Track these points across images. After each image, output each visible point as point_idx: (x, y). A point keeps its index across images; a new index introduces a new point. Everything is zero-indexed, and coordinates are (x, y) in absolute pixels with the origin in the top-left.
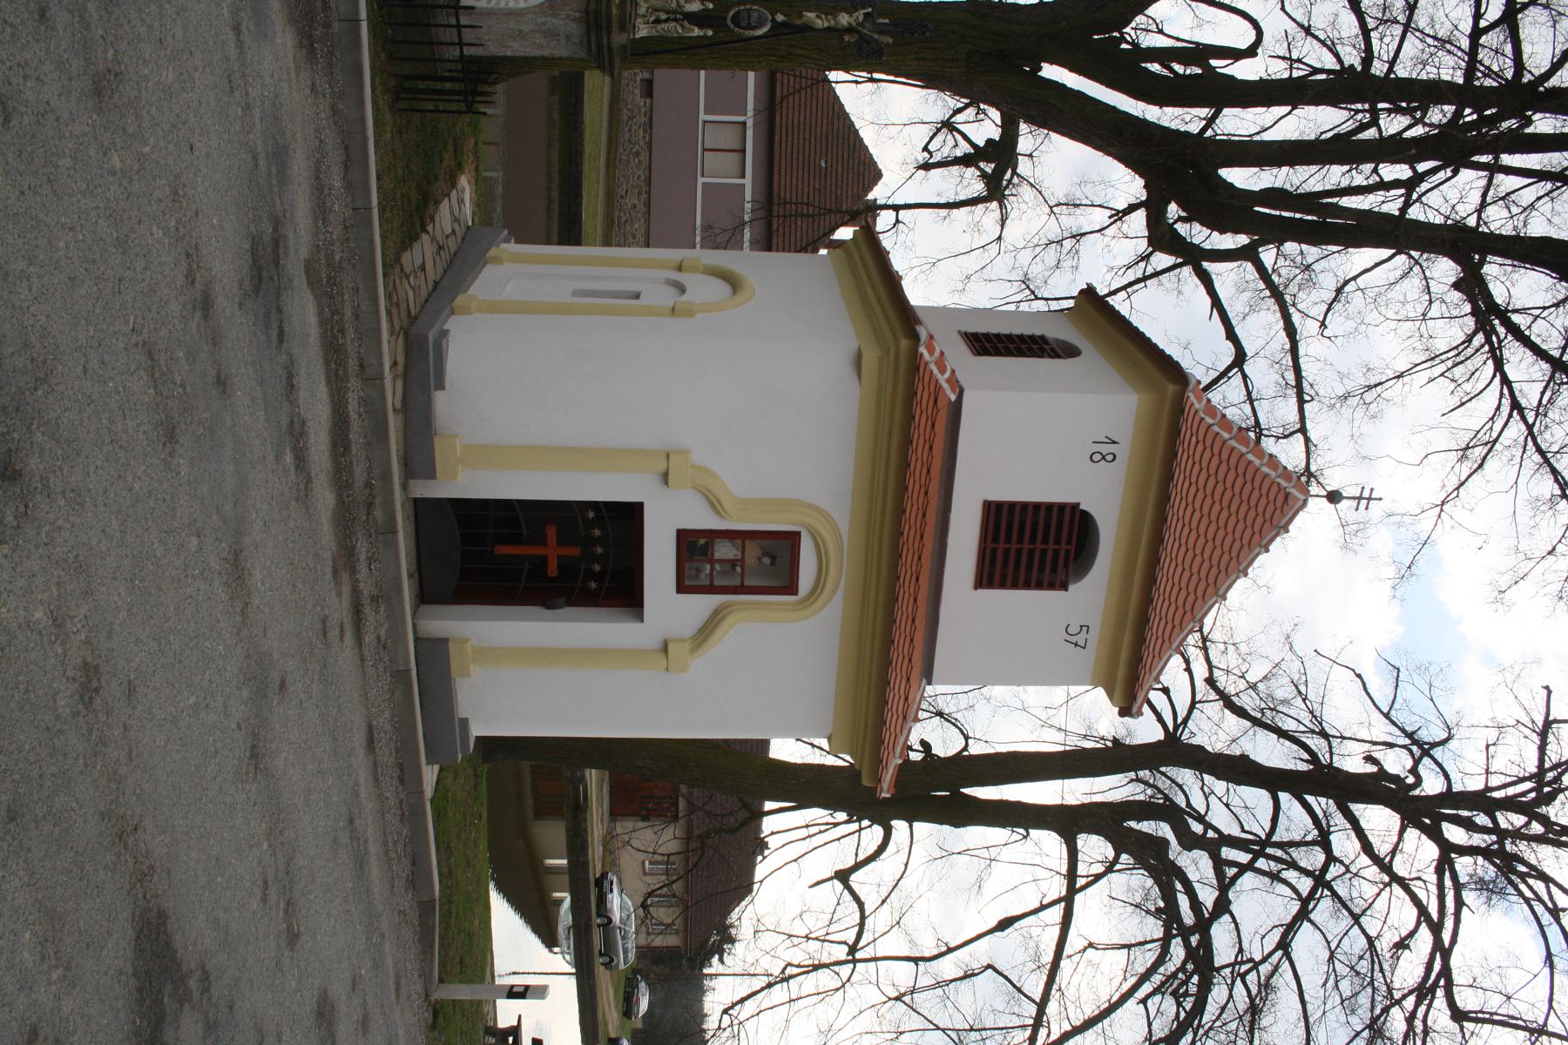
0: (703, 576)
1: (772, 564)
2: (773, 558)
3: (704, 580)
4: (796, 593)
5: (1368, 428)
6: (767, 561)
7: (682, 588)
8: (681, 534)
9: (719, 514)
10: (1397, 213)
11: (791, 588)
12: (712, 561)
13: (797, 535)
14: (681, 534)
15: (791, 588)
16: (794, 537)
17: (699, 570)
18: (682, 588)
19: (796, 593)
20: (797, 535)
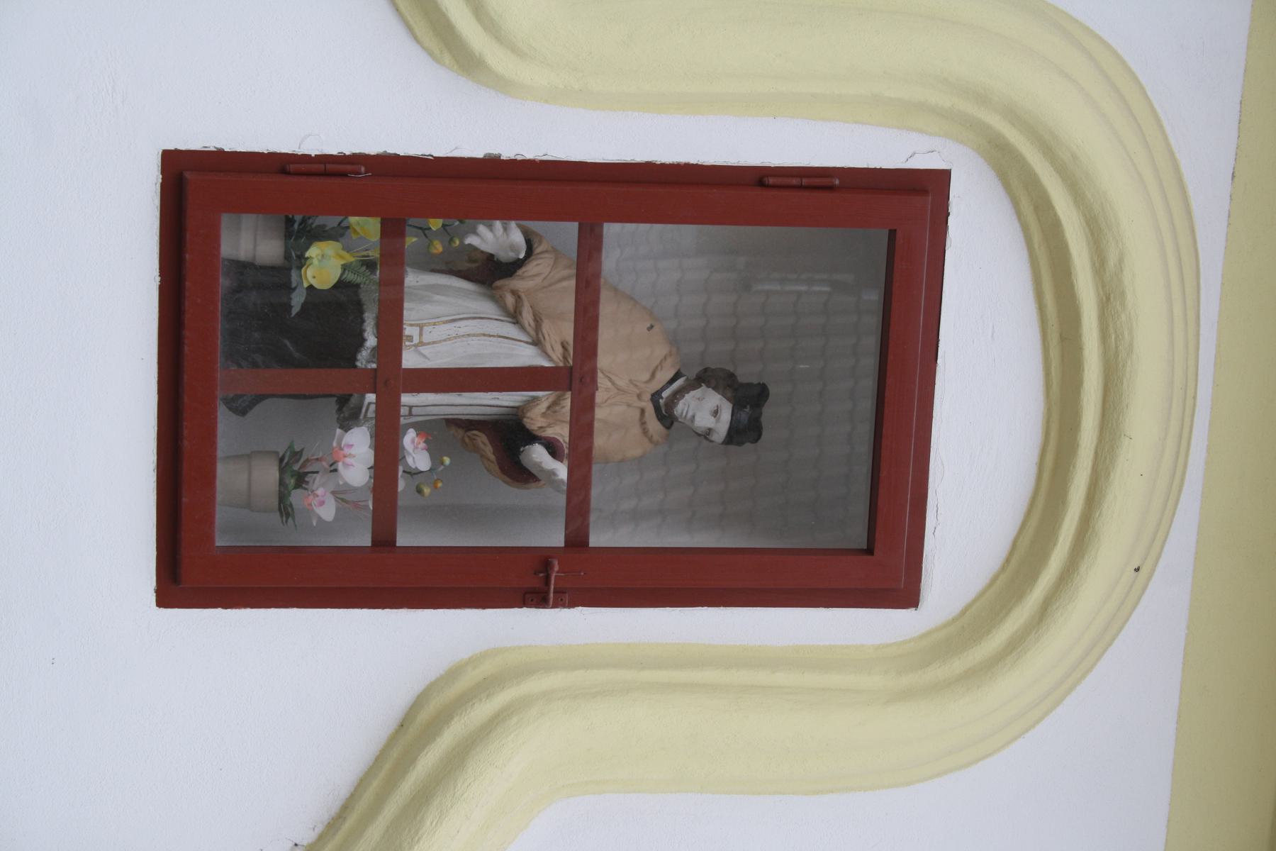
0: (322, 506)
1: (745, 431)
2: (749, 400)
3: (331, 510)
4: (900, 589)
5: (343, 262)
6: (708, 411)
7: (196, 565)
8: (196, 188)
9: (466, 62)
10: (611, 230)
11: (873, 558)
12: (393, 379)
13: (927, 190)
14: (196, 188)
15: (873, 558)
16: (894, 218)
17: (295, 473)
18: (196, 565)
19: (900, 589)
20: (927, 190)
